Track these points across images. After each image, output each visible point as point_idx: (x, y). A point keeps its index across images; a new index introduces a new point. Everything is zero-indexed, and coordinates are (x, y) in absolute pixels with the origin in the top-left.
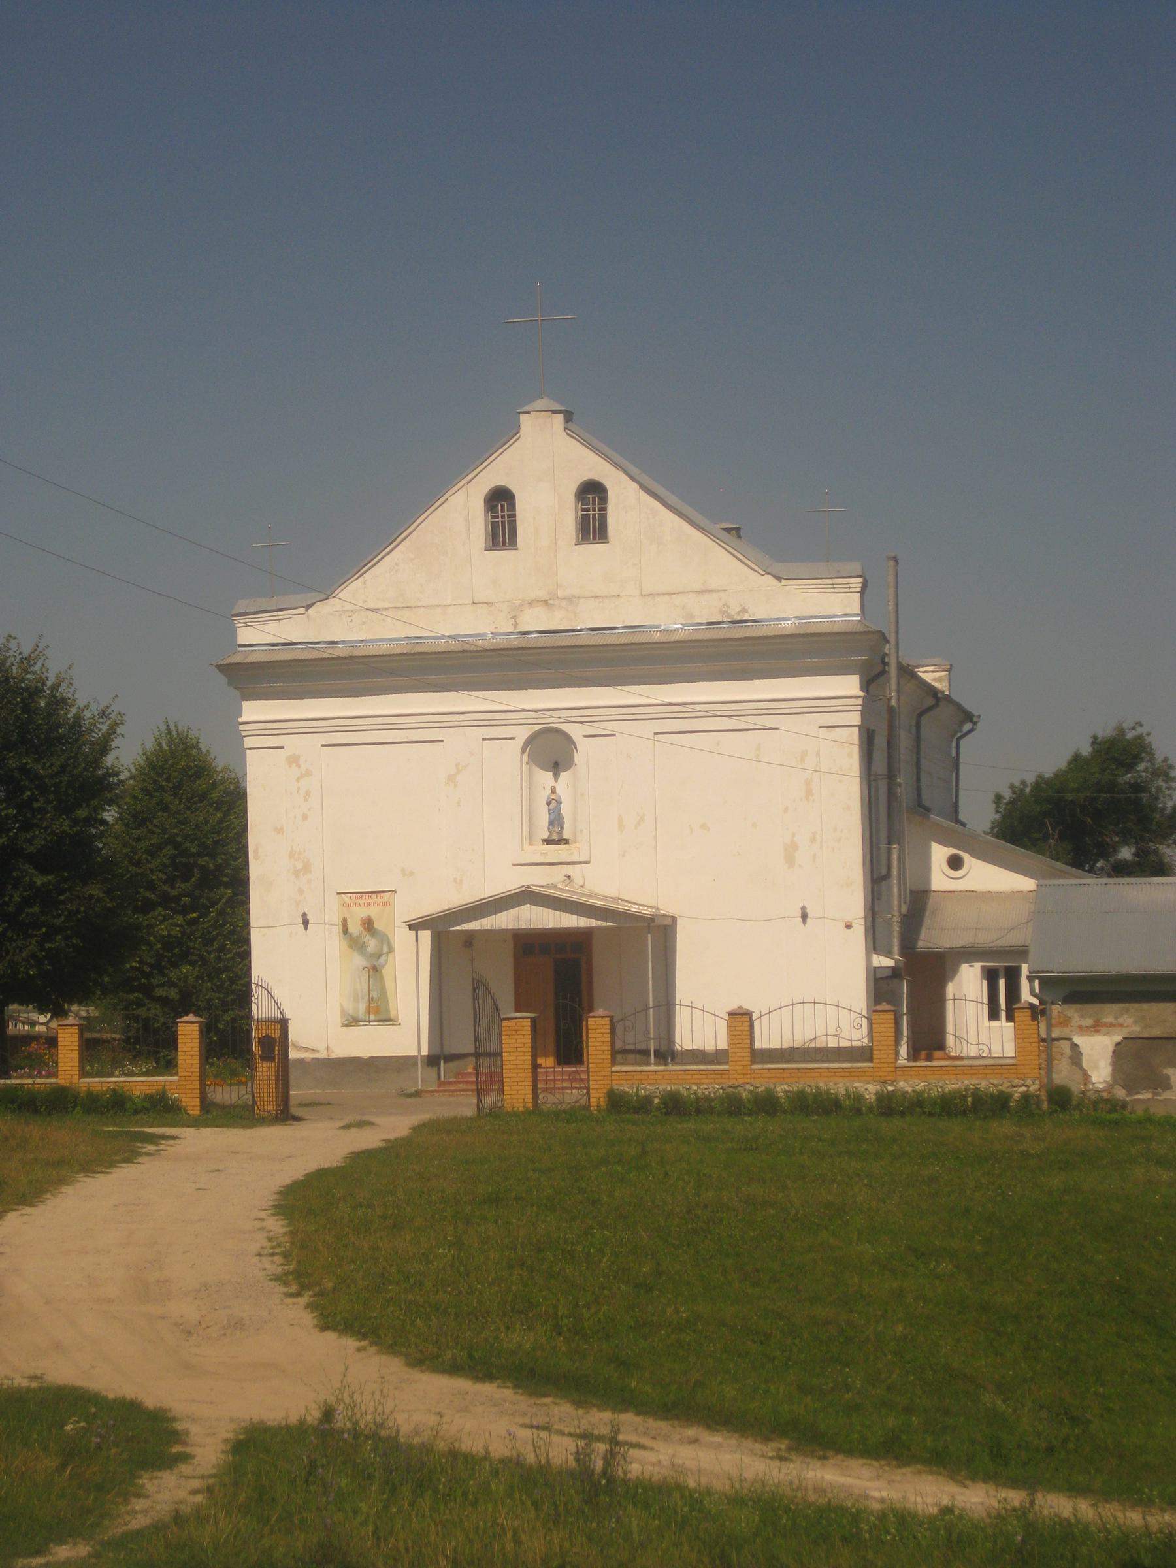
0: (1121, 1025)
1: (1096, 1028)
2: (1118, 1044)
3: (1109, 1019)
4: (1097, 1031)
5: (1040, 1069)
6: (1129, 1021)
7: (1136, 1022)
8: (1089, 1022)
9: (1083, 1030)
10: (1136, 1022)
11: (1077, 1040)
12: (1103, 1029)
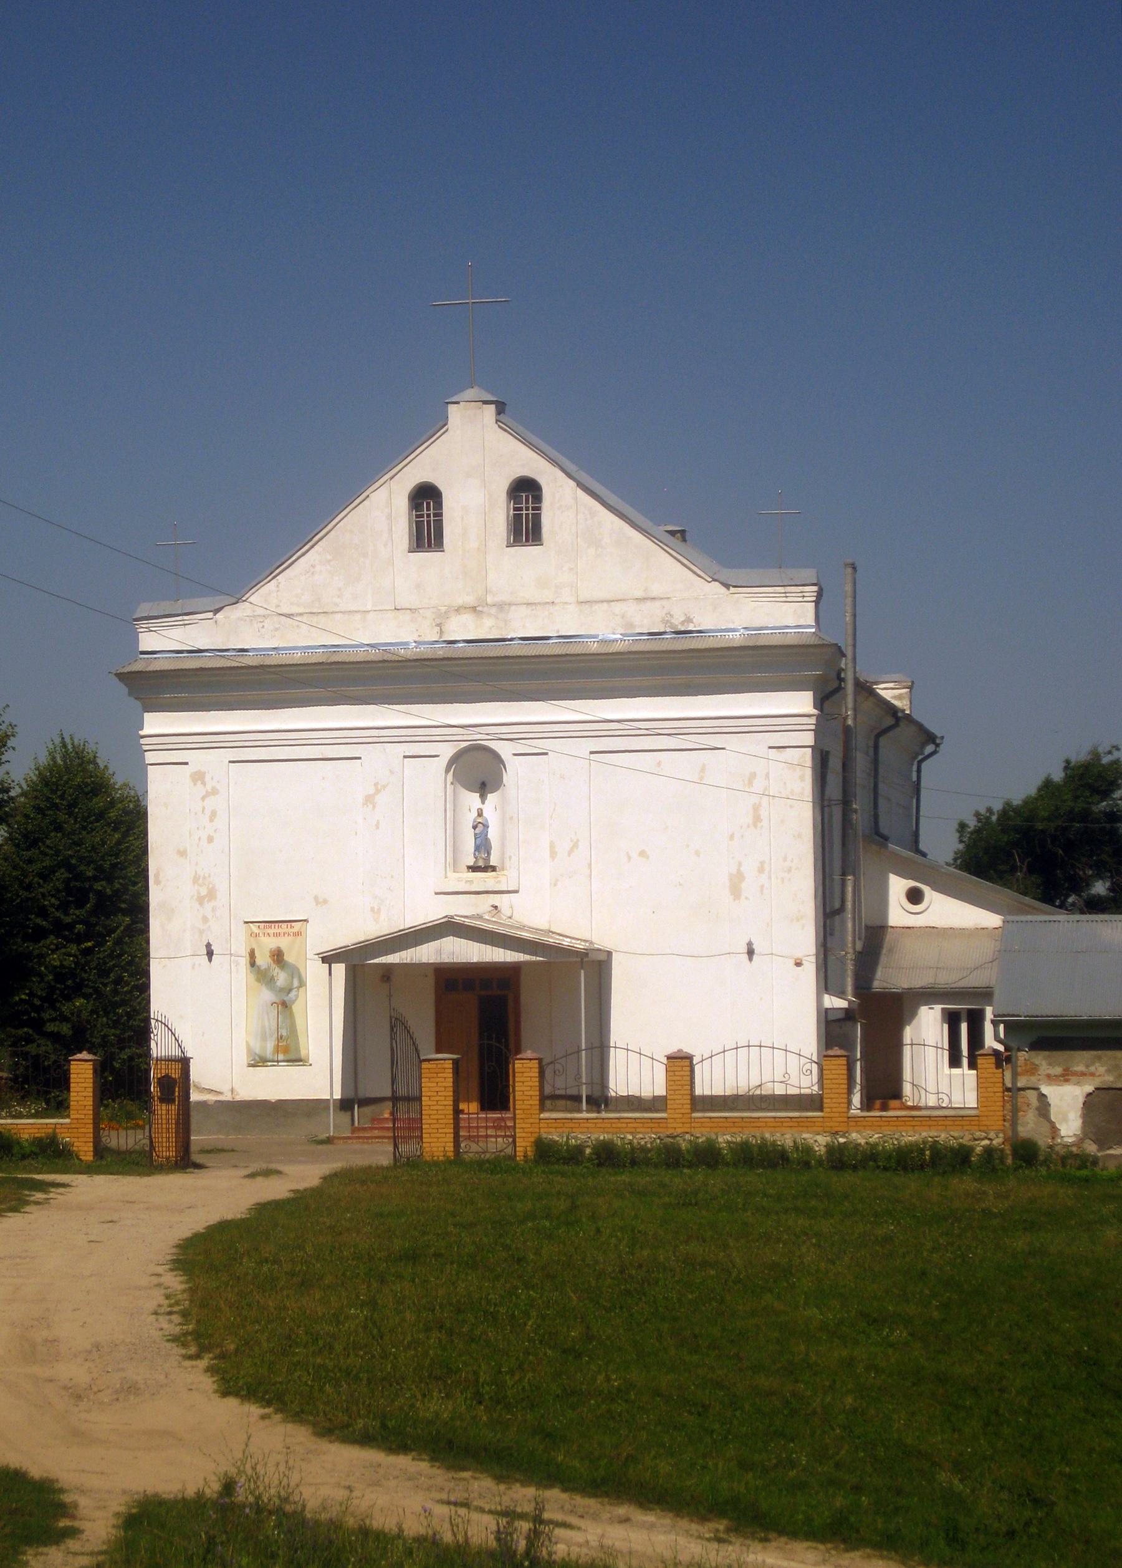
0: (1093, 1075)
1: (1065, 1077)
2: (1089, 1095)
3: (1081, 1068)
4: (1067, 1081)
5: (1004, 1120)
6: (1102, 1070)
7: (1108, 1071)
8: (1058, 1070)
9: (1051, 1079)
10: (1108, 1071)
11: (1045, 1090)
12: (1073, 1078)
